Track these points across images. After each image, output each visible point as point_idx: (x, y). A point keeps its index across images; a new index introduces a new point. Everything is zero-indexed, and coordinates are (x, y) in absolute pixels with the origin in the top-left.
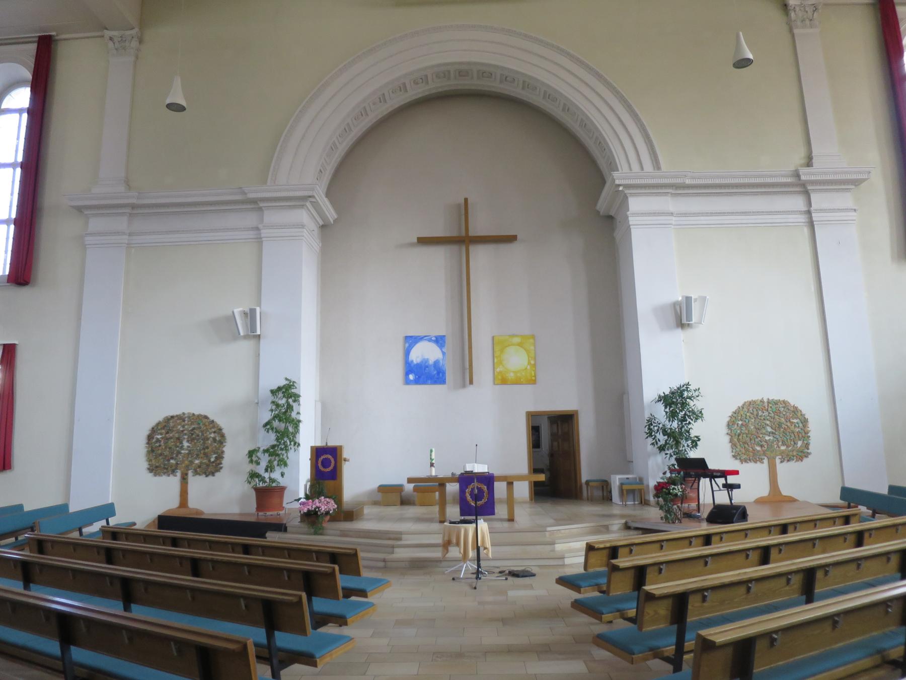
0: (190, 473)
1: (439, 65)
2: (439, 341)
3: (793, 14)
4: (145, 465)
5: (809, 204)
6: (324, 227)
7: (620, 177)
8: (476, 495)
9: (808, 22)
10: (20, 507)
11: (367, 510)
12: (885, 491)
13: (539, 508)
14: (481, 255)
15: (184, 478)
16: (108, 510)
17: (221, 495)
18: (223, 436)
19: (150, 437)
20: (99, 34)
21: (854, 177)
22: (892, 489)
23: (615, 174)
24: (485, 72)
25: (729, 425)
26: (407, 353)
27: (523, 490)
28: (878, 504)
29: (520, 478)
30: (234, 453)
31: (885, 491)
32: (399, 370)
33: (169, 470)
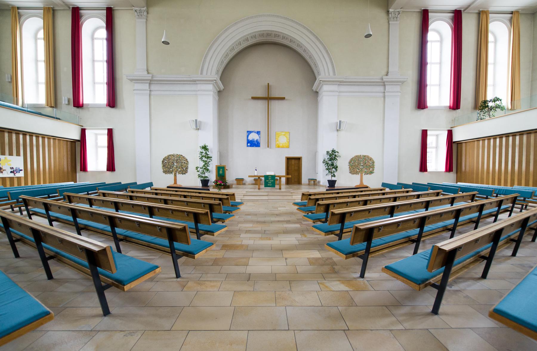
0: (177, 173)
1: (260, 31)
2: (258, 133)
3: (390, 15)
4: (162, 170)
5: (385, 89)
6: (219, 92)
7: (319, 78)
8: (270, 181)
9: (395, 19)
10: (120, 183)
11: (233, 186)
12: (396, 184)
13: (288, 186)
14: (275, 104)
15: (175, 175)
16: (150, 185)
17: (190, 180)
18: (188, 162)
19: (163, 162)
20: (131, 8)
21: (402, 80)
22: (413, 183)
23: (320, 77)
24: (277, 35)
25: (350, 163)
26: (248, 136)
27: (283, 180)
28: (391, 186)
29: (283, 176)
30: (191, 168)
31: (396, 184)
32: (245, 142)
33: (357, 173)
